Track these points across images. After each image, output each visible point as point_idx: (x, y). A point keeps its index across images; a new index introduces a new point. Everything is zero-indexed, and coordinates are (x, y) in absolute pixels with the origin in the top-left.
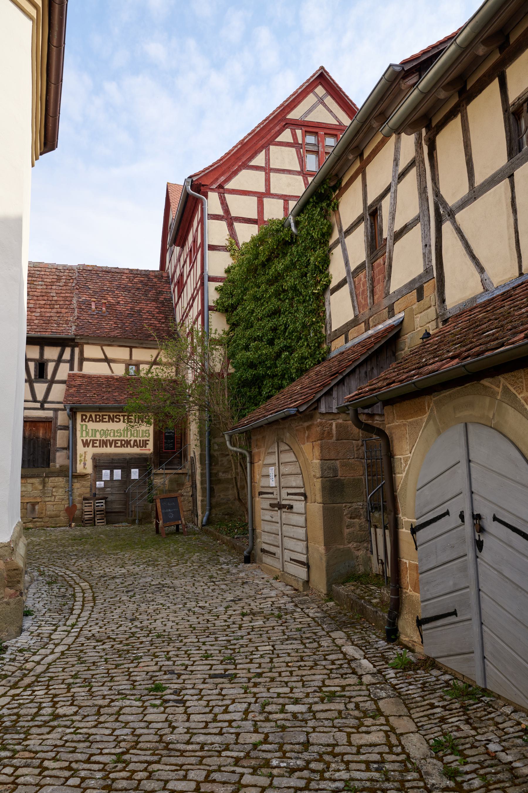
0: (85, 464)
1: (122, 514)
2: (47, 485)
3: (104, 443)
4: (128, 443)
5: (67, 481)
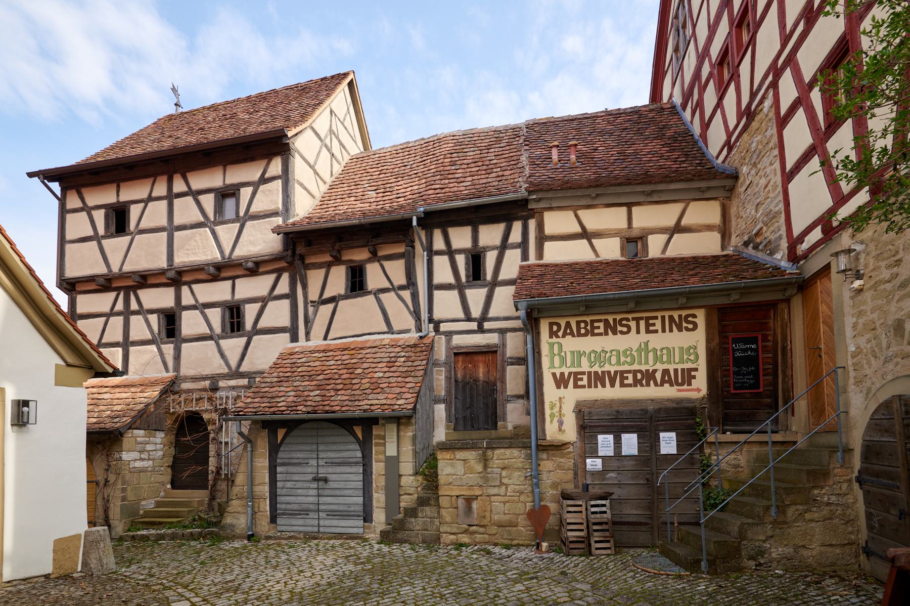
0: (561, 423)
1: (643, 528)
2: (491, 464)
3: (598, 379)
4: (649, 377)
5: (529, 457)
